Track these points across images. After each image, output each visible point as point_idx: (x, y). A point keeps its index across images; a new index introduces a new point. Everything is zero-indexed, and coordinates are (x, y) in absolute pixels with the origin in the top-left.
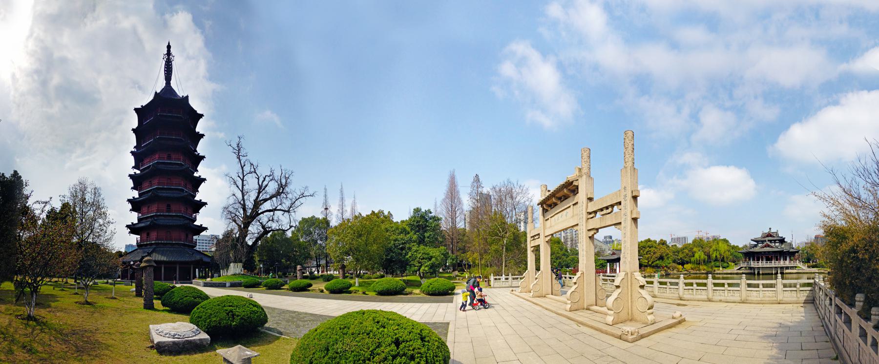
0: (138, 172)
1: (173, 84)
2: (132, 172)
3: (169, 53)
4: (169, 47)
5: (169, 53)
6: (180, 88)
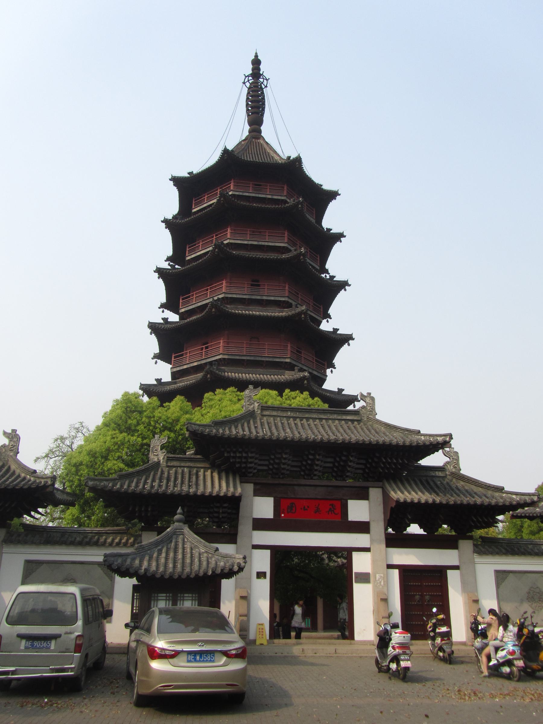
0: (174, 318)
2: (166, 265)
3: (256, 73)
4: (256, 62)
5: (256, 73)
6: (282, 139)
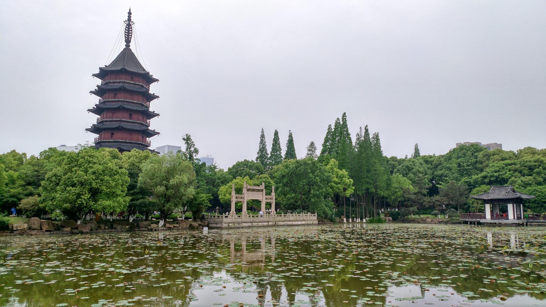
1: (132, 47)
4: (130, 13)
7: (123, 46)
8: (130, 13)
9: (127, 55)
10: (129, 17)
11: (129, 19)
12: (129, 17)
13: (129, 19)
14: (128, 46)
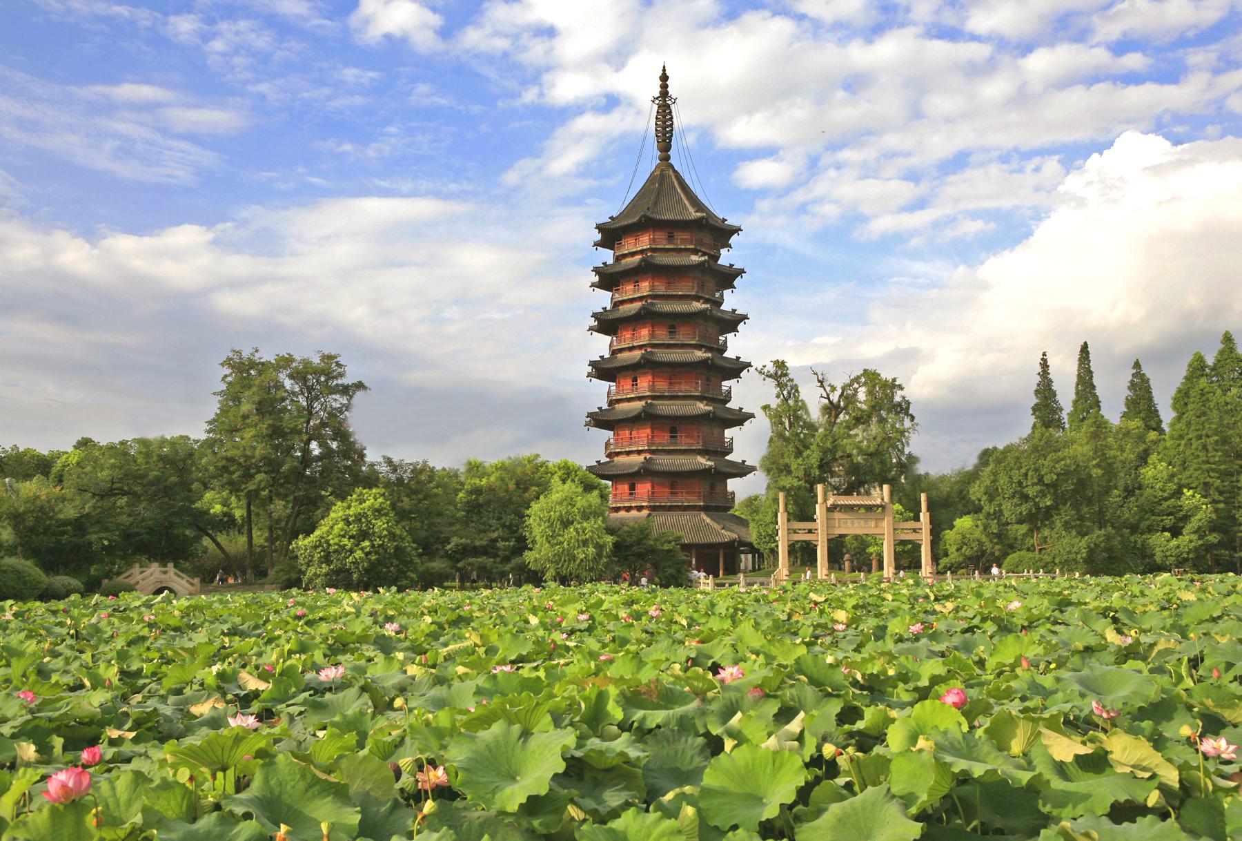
4: (664, 78)
7: (651, 160)
8: (664, 78)
9: (665, 180)
10: (664, 87)
11: (664, 93)
12: (664, 87)
13: (664, 93)
14: (665, 158)
